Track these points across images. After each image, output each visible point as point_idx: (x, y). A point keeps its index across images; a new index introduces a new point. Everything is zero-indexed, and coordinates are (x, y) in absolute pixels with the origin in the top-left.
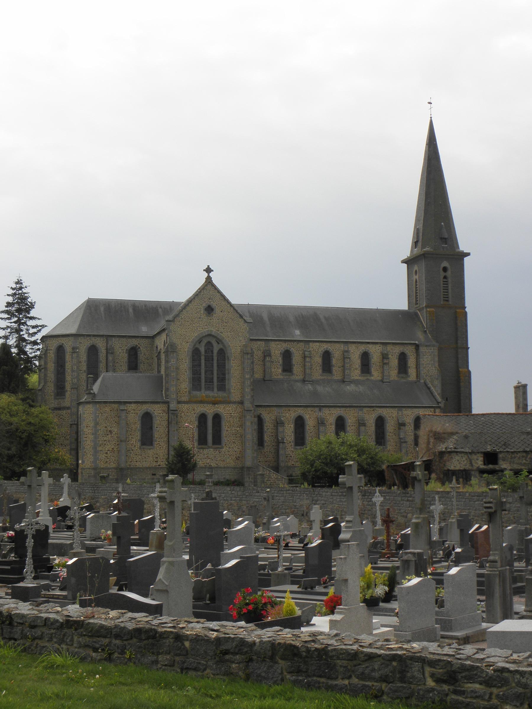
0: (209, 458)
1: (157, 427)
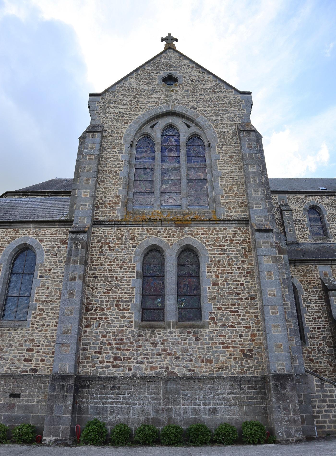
0: (170, 354)
1: (41, 277)
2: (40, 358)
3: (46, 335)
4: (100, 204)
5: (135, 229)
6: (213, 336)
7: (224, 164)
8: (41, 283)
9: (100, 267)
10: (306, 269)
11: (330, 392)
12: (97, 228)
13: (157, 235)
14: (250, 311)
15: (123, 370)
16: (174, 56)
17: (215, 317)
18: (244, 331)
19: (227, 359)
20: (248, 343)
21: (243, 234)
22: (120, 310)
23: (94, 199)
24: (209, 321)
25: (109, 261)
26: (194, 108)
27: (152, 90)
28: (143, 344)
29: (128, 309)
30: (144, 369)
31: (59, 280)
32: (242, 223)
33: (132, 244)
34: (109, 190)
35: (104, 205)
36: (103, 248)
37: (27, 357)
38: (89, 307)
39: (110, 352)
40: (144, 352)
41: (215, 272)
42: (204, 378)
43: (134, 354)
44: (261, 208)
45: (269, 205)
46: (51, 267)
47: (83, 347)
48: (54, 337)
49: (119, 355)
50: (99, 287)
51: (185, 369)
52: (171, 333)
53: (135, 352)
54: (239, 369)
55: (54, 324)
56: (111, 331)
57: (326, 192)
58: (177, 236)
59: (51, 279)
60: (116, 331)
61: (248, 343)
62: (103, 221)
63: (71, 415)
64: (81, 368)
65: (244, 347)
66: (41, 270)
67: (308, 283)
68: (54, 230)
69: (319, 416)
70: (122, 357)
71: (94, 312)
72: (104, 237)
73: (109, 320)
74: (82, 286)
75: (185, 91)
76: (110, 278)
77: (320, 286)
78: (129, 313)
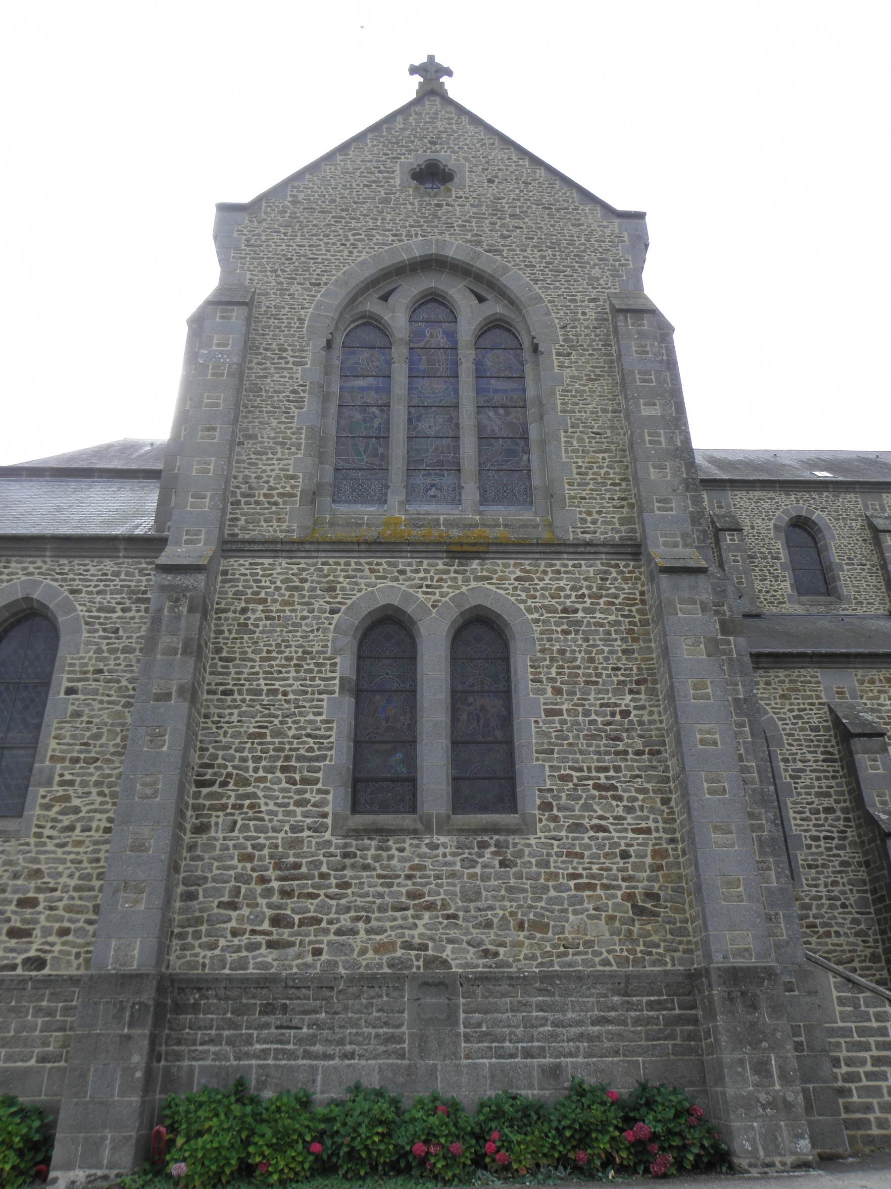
0: (430, 907)
1: (70, 691)
2: (57, 925)
3: (79, 857)
4: (244, 495)
5: (338, 564)
6: (549, 855)
7: (575, 396)
8: (71, 708)
9: (238, 666)
10: (787, 680)
11: (877, 1020)
12: (233, 560)
13: (396, 579)
14: (649, 786)
15: (299, 956)
16: (443, 113)
17: (554, 803)
18: (634, 842)
19: (588, 921)
20: (645, 875)
21: (625, 580)
22: (294, 783)
23: (227, 482)
24: (537, 812)
25: (265, 649)
26: (496, 251)
27: (385, 201)
28: (357, 877)
29: (317, 781)
30: (357, 950)
31: (123, 700)
32: (622, 550)
33: (328, 603)
34: (268, 459)
35: (253, 500)
36: (249, 614)
37: (18, 925)
38: (205, 774)
39: (263, 902)
40: (358, 903)
41: (553, 680)
42: (525, 977)
43: (330, 907)
44: (674, 513)
45: (693, 504)
46: (101, 665)
47: (185, 888)
48: (102, 864)
49: (289, 912)
50: (235, 718)
51: (472, 950)
52: (434, 846)
53: (334, 902)
54: (622, 950)
55: (104, 824)
56: (267, 843)
57: (832, 482)
58: (450, 583)
59: (99, 697)
60: (279, 841)
61: (645, 875)
62: (249, 542)
63: (142, 1097)
64: (178, 953)
65: (636, 887)
66: (70, 672)
67: (795, 717)
68: (112, 563)
69: (850, 1090)
70: (296, 918)
71: (220, 790)
72: (252, 583)
73: (260, 812)
74: (189, 716)
75: (472, 205)
76: (267, 695)
77: (825, 724)
78: (319, 791)
